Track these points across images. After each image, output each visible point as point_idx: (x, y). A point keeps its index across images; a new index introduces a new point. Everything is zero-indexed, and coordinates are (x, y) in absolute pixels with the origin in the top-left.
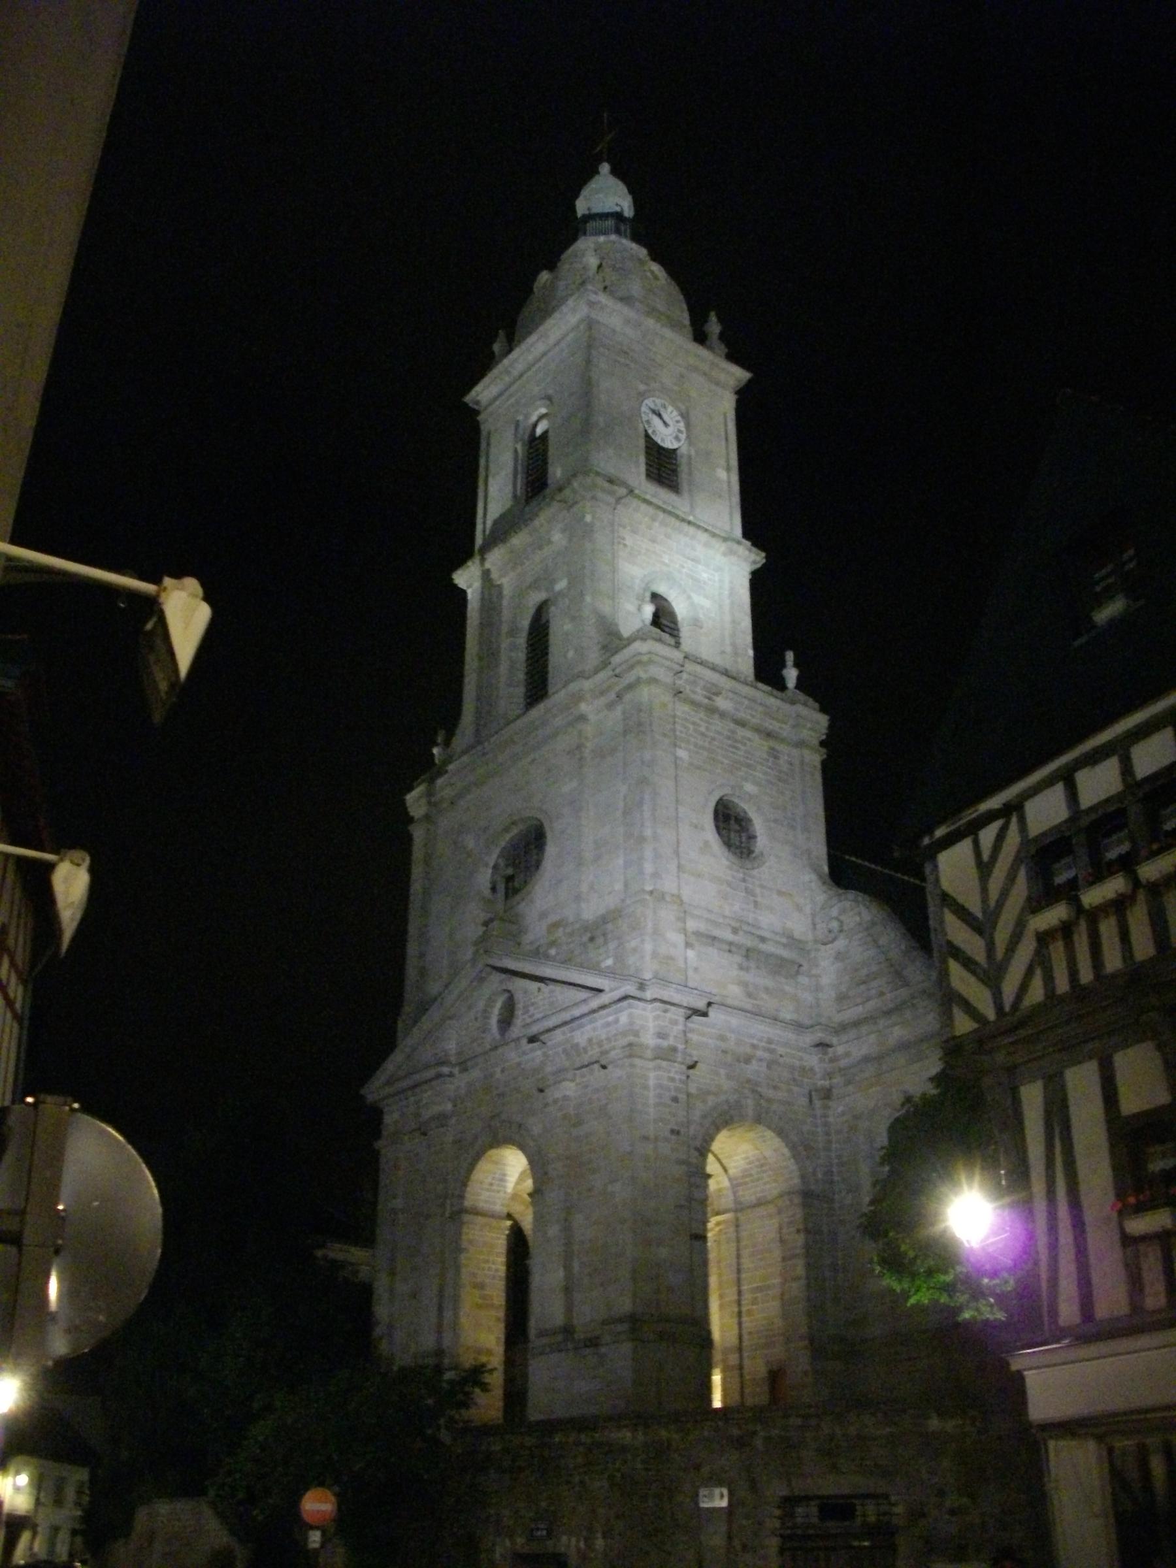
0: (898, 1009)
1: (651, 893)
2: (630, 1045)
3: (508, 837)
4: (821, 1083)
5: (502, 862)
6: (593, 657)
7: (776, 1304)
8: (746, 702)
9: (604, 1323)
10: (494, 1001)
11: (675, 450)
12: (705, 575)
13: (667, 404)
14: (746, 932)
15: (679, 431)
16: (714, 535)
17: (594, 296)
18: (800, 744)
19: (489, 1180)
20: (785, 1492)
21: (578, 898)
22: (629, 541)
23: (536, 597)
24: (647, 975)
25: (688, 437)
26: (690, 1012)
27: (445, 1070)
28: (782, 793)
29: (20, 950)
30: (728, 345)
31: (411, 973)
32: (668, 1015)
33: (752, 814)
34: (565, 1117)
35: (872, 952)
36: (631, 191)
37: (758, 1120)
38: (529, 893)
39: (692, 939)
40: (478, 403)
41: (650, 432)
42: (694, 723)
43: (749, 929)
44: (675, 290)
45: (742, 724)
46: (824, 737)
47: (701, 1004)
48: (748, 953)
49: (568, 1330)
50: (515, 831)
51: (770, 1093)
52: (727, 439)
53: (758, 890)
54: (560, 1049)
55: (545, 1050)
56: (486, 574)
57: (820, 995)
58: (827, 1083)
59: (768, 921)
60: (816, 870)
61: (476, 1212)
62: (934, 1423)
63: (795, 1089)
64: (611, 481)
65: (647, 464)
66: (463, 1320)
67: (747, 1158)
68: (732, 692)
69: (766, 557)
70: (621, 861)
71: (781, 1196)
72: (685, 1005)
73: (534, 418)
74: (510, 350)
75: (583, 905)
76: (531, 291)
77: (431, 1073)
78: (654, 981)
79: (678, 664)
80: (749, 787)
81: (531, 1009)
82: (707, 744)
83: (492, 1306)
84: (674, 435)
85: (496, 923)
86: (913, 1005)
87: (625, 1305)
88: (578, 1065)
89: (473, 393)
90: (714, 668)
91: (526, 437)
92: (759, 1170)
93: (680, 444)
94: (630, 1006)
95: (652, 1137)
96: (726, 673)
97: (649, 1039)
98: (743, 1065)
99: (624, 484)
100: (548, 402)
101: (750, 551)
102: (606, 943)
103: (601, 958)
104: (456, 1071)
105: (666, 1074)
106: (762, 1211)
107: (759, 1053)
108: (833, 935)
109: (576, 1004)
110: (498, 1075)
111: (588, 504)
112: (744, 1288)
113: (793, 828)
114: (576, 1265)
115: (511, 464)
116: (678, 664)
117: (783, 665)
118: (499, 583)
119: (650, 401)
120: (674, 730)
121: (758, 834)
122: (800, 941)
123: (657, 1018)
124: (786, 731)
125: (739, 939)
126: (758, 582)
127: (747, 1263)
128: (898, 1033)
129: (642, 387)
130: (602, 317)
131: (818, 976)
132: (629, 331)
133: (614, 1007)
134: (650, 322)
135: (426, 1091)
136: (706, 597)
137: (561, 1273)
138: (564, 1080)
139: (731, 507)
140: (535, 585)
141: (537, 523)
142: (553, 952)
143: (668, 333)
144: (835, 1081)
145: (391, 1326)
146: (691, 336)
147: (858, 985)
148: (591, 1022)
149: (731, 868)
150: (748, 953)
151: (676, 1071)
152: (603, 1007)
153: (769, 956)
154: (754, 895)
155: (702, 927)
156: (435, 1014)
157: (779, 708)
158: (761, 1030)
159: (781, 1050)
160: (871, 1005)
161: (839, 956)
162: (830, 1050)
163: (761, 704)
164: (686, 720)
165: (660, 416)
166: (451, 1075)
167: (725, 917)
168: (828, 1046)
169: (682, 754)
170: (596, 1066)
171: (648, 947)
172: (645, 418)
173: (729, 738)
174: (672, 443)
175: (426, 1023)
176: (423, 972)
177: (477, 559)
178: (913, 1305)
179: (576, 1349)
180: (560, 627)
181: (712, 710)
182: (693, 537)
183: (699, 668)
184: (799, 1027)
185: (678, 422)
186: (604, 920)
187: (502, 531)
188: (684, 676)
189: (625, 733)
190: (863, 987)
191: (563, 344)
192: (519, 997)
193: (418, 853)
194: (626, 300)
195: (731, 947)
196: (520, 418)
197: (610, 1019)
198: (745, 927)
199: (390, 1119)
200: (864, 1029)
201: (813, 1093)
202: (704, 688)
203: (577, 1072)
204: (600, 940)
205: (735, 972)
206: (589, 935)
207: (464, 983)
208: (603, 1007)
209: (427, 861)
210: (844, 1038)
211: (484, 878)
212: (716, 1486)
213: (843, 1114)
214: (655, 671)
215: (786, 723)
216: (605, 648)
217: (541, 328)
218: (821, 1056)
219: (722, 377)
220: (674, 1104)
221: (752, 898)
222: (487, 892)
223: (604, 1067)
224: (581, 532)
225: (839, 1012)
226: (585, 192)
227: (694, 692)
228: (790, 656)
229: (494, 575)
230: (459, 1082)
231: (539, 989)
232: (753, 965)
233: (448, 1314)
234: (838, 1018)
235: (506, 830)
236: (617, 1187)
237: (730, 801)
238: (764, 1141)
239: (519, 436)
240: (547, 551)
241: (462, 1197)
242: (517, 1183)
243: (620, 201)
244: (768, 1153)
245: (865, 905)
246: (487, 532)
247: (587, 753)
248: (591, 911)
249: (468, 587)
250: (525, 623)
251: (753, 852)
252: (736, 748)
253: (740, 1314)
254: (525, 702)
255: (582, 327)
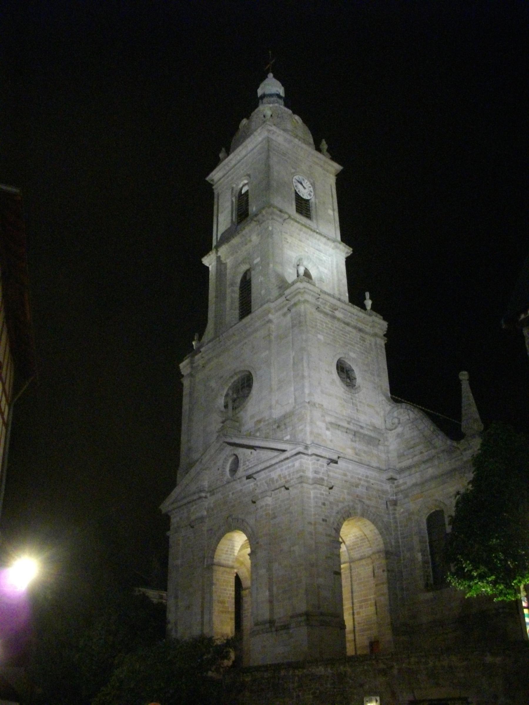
0: (431, 459)
1: (309, 403)
2: (301, 477)
3: (232, 381)
4: (391, 498)
5: (230, 392)
6: (275, 292)
7: (373, 609)
8: (349, 314)
9: (292, 617)
10: (228, 460)
11: (308, 201)
12: (324, 258)
13: (304, 179)
14: (354, 424)
15: (311, 191)
16: (328, 239)
17: (270, 127)
18: (375, 335)
19: (226, 549)
20: (411, 698)
21: (271, 407)
22: (289, 240)
23: (244, 268)
24: (309, 442)
25: (315, 194)
26: (329, 461)
27: (203, 494)
28: (367, 358)
29: (8, 381)
30: (331, 154)
31: (184, 448)
32: (319, 462)
33: (354, 367)
34: (266, 515)
35: (416, 433)
36: (283, 85)
37: (363, 515)
38: (244, 407)
39: (329, 427)
40: (213, 180)
41: (297, 191)
42: (326, 323)
43: (356, 422)
44: (306, 128)
45: (348, 324)
46: (385, 333)
47: (335, 457)
48: (355, 433)
49: (271, 622)
50: (236, 378)
51: (367, 502)
52: (332, 196)
53: (359, 404)
54: (264, 481)
55: (256, 482)
56: (218, 258)
57: (389, 455)
58: (395, 498)
59: (363, 419)
60: (385, 395)
61: (220, 565)
62: (489, 659)
63: (380, 501)
64: (281, 211)
65: (296, 206)
66: (214, 619)
67: (355, 536)
68: (343, 309)
69: (353, 251)
70: (292, 389)
71: (374, 553)
72: (328, 457)
73: (241, 186)
74: (228, 155)
75: (273, 411)
76: (238, 128)
77: (195, 497)
78: (313, 444)
79: (318, 294)
80: (352, 355)
81: (247, 463)
82: (332, 333)
83: (229, 612)
84: (308, 193)
85: (228, 422)
86: (438, 457)
87: (303, 607)
88: (273, 489)
89: (210, 175)
90: (333, 297)
91: (237, 194)
92: (361, 541)
93: (311, 197)
94: (301, 458)
95: (313, 523)
96: (339, 300)
97: (310, 474)
98: (355, 488)
99: (286, 213)
100: (248, 178)
101: (345, 247)
102: (286, 428)
103: (284, 435)
104: (208, 495)
105: (319, 492)
106: (363, 562)
107: (362, 482)
108: (395, 426)
109: (271, 459)
110: (231, 496)
111: (270, 222)
112: (355, 601)
113: (374, 375)
114: (275, 589)
115: (229, 209)
116: (318, 294)
117: (365, 299)
118: (225, 262)
119: (296, 177)
120: (316, 325)
121: (357, 377)
122: (379, 429)
123: (314, 464)
124: (368, 329)
125: (351, 427)
126: (349, 262)
127: (355, 587)
128: (431, 472)
129: (293, 171)
130: (274, 137)
131: (388, 446)
132: (287, 145)
133: (293, 458)
134: (296, 141)
135: (193, 506)
136: (326, 268)
137: (267, 593)
138: (267, 496)
139: (335, 228)
140: (243, 262)
141: (244, 232)
142: (258, 434)
143: (304, 146)
144: (398, 497)
145: (176, 624)
146: (314, 148)
147: (409, 449)
148: (279, 467)
149: (345, 393)
150: (355, 433)
151: (324, 490)
152: (287, 458)
153: (365, 435)
154: (356, 406)
155: (333, 420)
156: (198, 467)
157: (364, 318)
158: (362, 471)
159: (372, 481)
160: (416, 459)
161: (398, 435)
162: (396, 481)
163: (356, 315)
164: (322, 321)
165: (301, 184)
166: (206, 497)
167: (343, 416)
168: (396, 479)
169: (320, 337)
170: (283, 489)
171: (308, 429)
172: (294, 184)
173: (341, 330)
174: (307, 196)
175: (193, 472)
176: (190, 449)
177: (214, 251)
178: (468, 598)
179: (276, 631)
180: (257, 280)
181: (334, 317)
182: (319, 240)
183: (327, 297)
184: (379, 469)
185: (310, 187)
186: (285, 417)
187: (226, 238)
188: (321, 300)
189: (293, 326)
190: (412, 450)
191: (255, 151)
192: (240, 457)
193: (186, 391)
194: (285, 130)
195: (347, 431)
196: (234, 186)
197: (290, 465)
198: (353, 421)
199: (174, 520)
200: (413, 470)
201: (388, 503)
202: (330, 307)
203: (273, 492)
204: (283, 427)
205: (349, 443)
206: (277, 425)
207: (213, 451)
208: (287, 458)
209: (191, 394)
210: (403, 475)
211: (221, 401)
212: (373, 695)
213: (403, 513)
214: (307, 297)
215: (367, 325)
216: (280, 288)
217: (244, 144)
218: (391, 484)
219: (330, 168)
220: (323, 506)
221: (356, 408)
222: (223, 409)
223: (287, 489)
224: (266, 235)
225: (399, 463)
226: (262, 86)
227: (324, 308)
228: (367, 295)
229: (223, 259)
230: (210, 501)
231: (251, 453)
232: (357, 439)
233: (206, 617)
234: (399, 466)
235: (232, 377)
236: (296, 548)
237: (345, 361)
238: (365, 526)
239: (234, 194)
240: (249, 246)
241: (213, 558)
242: (239, 551)
243: (278, 89)
244: (367, 532)
245: (411, 410)
246: (219, 239)
247: (272, 337)
248: (277, 413)
249: (209, 265)
250: (238, 280)
251: (355, 386)
252: (346, 336)
253: (353, 614)
254: (239, 317)
255: (264, 142)
